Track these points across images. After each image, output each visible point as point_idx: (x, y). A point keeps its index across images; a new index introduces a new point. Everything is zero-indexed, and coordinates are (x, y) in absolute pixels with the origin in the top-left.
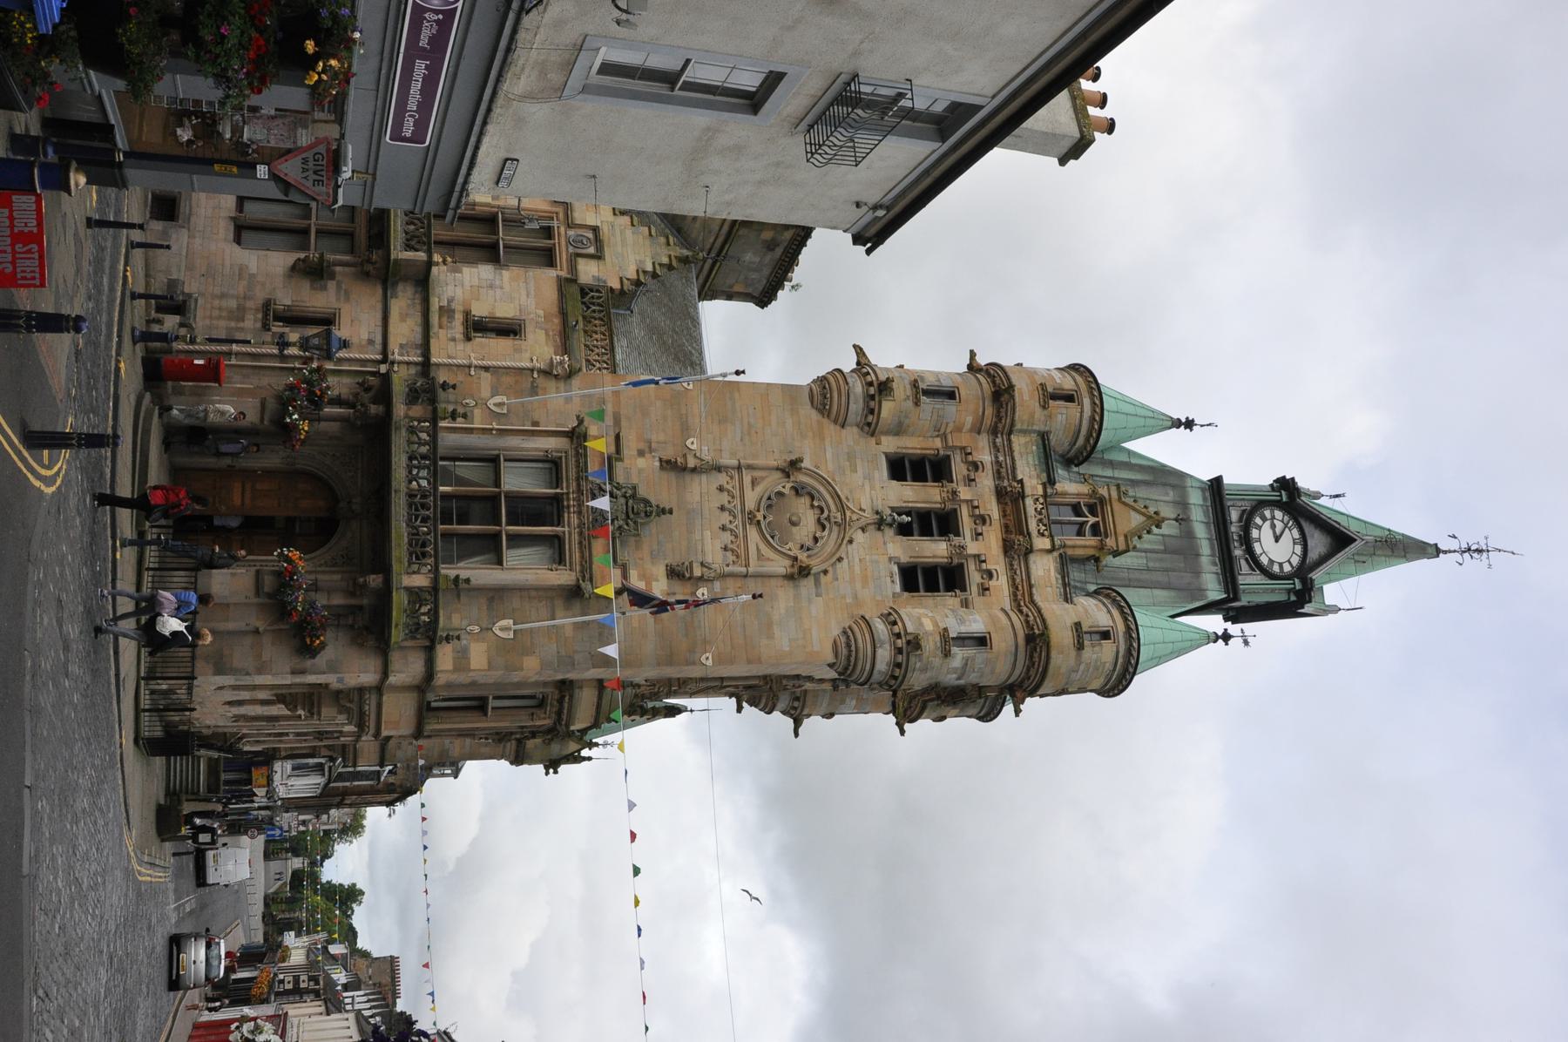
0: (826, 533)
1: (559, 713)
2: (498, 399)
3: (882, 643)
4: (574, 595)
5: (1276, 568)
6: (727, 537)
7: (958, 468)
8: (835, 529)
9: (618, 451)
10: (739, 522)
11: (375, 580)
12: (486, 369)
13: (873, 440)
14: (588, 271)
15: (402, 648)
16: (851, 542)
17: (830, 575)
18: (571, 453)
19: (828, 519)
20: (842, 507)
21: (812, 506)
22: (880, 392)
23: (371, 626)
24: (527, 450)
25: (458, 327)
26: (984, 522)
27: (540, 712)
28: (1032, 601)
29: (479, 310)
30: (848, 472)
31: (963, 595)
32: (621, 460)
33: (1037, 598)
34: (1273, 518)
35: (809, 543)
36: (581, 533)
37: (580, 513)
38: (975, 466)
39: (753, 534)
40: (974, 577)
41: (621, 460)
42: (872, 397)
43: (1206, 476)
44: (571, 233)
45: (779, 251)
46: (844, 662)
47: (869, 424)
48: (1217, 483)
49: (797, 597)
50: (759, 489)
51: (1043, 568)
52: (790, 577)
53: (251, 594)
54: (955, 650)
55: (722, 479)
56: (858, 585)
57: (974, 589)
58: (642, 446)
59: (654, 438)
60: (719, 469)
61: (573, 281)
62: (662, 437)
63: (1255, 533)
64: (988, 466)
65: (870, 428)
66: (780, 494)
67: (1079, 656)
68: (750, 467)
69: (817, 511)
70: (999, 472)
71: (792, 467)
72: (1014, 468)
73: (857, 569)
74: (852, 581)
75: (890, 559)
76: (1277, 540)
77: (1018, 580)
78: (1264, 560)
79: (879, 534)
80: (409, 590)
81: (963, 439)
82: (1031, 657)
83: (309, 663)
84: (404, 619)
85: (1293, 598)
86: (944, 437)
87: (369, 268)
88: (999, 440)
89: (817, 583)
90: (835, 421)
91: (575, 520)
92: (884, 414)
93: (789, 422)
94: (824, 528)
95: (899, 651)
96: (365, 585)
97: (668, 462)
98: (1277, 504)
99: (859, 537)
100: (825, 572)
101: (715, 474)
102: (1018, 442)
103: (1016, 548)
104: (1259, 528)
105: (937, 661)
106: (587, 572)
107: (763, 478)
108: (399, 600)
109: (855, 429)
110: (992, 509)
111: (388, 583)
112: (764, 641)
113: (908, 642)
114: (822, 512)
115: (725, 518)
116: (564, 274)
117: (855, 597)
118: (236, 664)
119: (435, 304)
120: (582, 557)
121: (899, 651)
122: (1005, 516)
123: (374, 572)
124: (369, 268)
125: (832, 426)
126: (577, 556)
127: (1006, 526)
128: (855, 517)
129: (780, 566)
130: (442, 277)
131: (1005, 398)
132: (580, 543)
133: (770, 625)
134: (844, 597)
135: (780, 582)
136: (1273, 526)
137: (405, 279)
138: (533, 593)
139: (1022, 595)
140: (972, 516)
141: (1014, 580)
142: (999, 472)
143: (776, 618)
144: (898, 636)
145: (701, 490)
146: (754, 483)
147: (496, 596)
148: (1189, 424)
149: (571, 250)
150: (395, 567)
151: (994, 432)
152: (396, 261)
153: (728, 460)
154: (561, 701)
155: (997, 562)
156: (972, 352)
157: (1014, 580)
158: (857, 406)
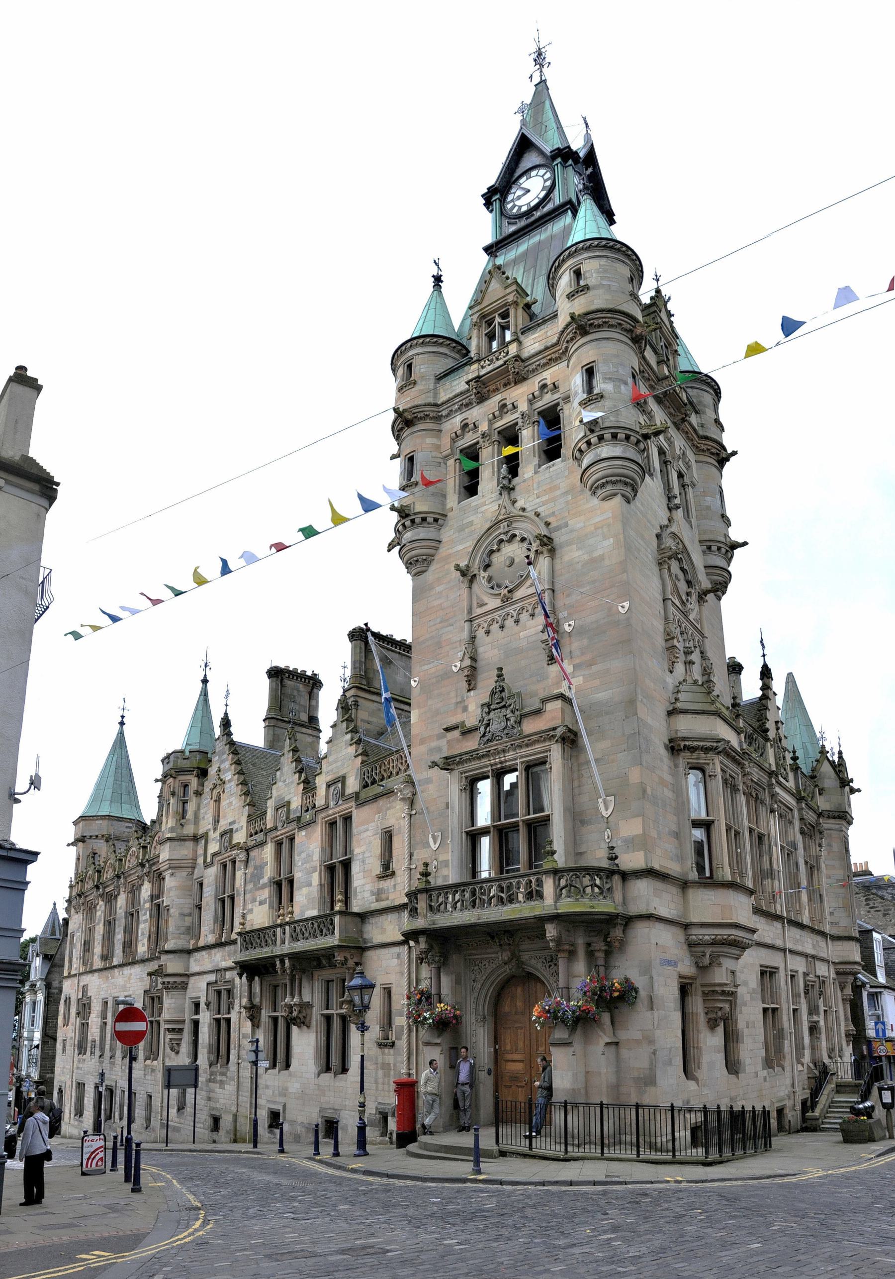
0: (517, 532)
1: (707, 750)
2: (431, 841)
3: (597, 455)
4: (570, 740)
5: (548, 183)
6: (524, 616)
7: (468, 439)
8: (514, 525)
9: (455, 728)
10: (511, 610)
11: (551, 931)
12: (411, 855)
13: (450, 514)
14: (353, 785)
15: (624, 903)
16: (524, 510)
17: (549, 520)
18: (461, 768)
19: (506, 533)
20: (498, 523)
21: (499, 550)
22: (407, 515)
23: (604, 932)
24: (460, 808)
25: (387, 884)
26: (505, 405)
27: (709, 770)
28: (557, 344)
29: (378, 870)
30: (473, 528)
31: (561, 403)
32: (463, 723)
33: (555, 340)
34: (512, 201)
35: (525, 544)
36: (520, 747)
37: (504, 751)
38: (465, 426)
39: (519, 594)
40: (548, 399)
41: (463, 723)
42: (413, 521)
43: (485, 257)
44: (332, 804)
45: (390, 655)
46: (620, 486)
47: (436, 520)
48: (488, 249)
49: (569, 543)
50: (486, 599)
51: (533, 343)
52: (552, 552)
53: (570, 1050)
54: (596, 391)
55: (480, 633)
56: (558, 493)
57: (556, 396)
58: (460, 710)
59: (454, 701)
60: (473, 638)
61: (357, 795)
62: (453, 694)
63: (524, 209)
64: (464, 416)
65: (439, 519)
66: (490, 580)
67: (596, 287)
68: (470, 611)
69: (503, 545)
70: (467, 405)
71: (467, 575)
72: (461, 393)
73: (544, 498)
74: (554, 500)
75: (536, 473)
76: (529, 191)
77: (544, 361)
78: (543, 193)
79: (517, 488)
80: (558, 897)
81: (446, 441)
82: (599, 326)
83: (643, 993)
84: (586, 900)
85: (570, 162)
86: (446, 458)
87: (351, 963)
88: (444, 413)
89: (558, 529)
90: (437, 549)
91: (510, 755)
92: (425, 508)
93: (439, 589)
94: (514, 536)
95: (601, 438)
96: (558, 941)
97: (469, 682)
98: (503, 201)
99: (520, 504)
100: (548, 524)
101: (477, 641)
102: (443, 397)
103: (517, 372)
104: (520, 207)
105: (607, 403)
106: (547, 735)
107: (478, 598)
108: (567, 905)
109: (442, 531)
110: (493, 403)
111: (556, 918)
112: (607, 562)
113: (592, 431)
114: (502, 541)
115: (510, 622)
116: (353, 804)
117: (566, 493)
118: (645, 1064)
119: (375, 906)
120: (538, 741)
121: (601, 438)
122: (497, 389)
123: (543, 935)
124: (351, 963)
125: (441, 550)
126: (538, 747)
127: (505, 385)
128: (503, 511)
129: (544, 562)
130: (360, 903)
131: (408, 416)
132: (527, 745)
133: (593, 561)
134: (567, 502)
135: (557, 561)
136: (519, 198)
137: (361, 932)
138: (576, 784)
139: (555, 354)
140: (501, 416)
141: (545, 365)
142: (467, 405)
143: (586, 557)
144: (589, 443)
145: (490, 651)
146: (481, 605)
147: (577, 818)
148: (438, 279)
149: (340, 802)
150: (537, 913)
151: (438, 419)
152: (340, 940)
153: (465, 635)
154: (692, 749)
155: (532, 385)
156: (392, 458)
157: (545, 365)
158: (422, 532)
